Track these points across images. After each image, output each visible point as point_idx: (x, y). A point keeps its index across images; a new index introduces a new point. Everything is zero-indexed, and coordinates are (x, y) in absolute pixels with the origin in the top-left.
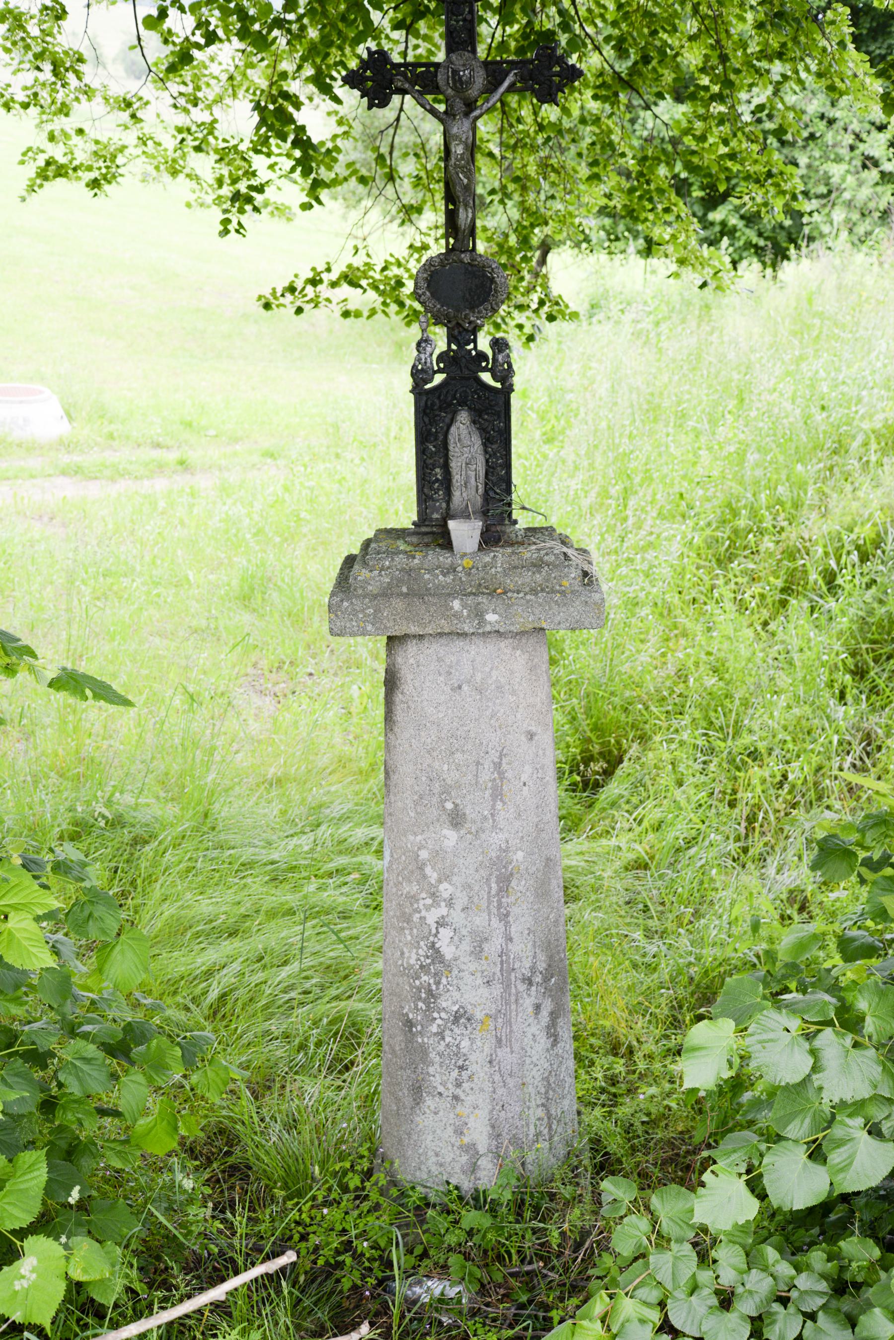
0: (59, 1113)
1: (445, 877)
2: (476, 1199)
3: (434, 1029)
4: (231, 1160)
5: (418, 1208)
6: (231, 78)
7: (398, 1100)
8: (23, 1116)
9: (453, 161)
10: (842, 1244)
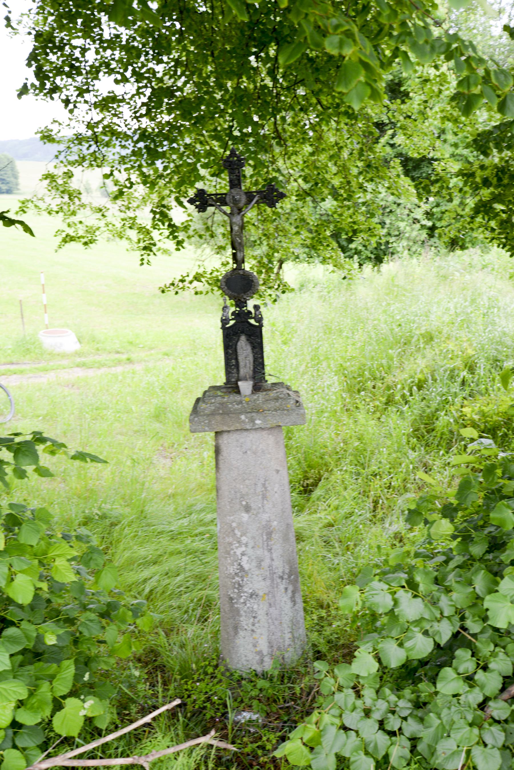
0: (80, 645)
1: (243, 534)
2: (263, 675)
3: (242, 600)
4: (157, 663)
5: (238, 681)
6: (143, 198)
7: (228, 633)
8: (63, 647)
9: (234, 233)
10: (419, 685)
